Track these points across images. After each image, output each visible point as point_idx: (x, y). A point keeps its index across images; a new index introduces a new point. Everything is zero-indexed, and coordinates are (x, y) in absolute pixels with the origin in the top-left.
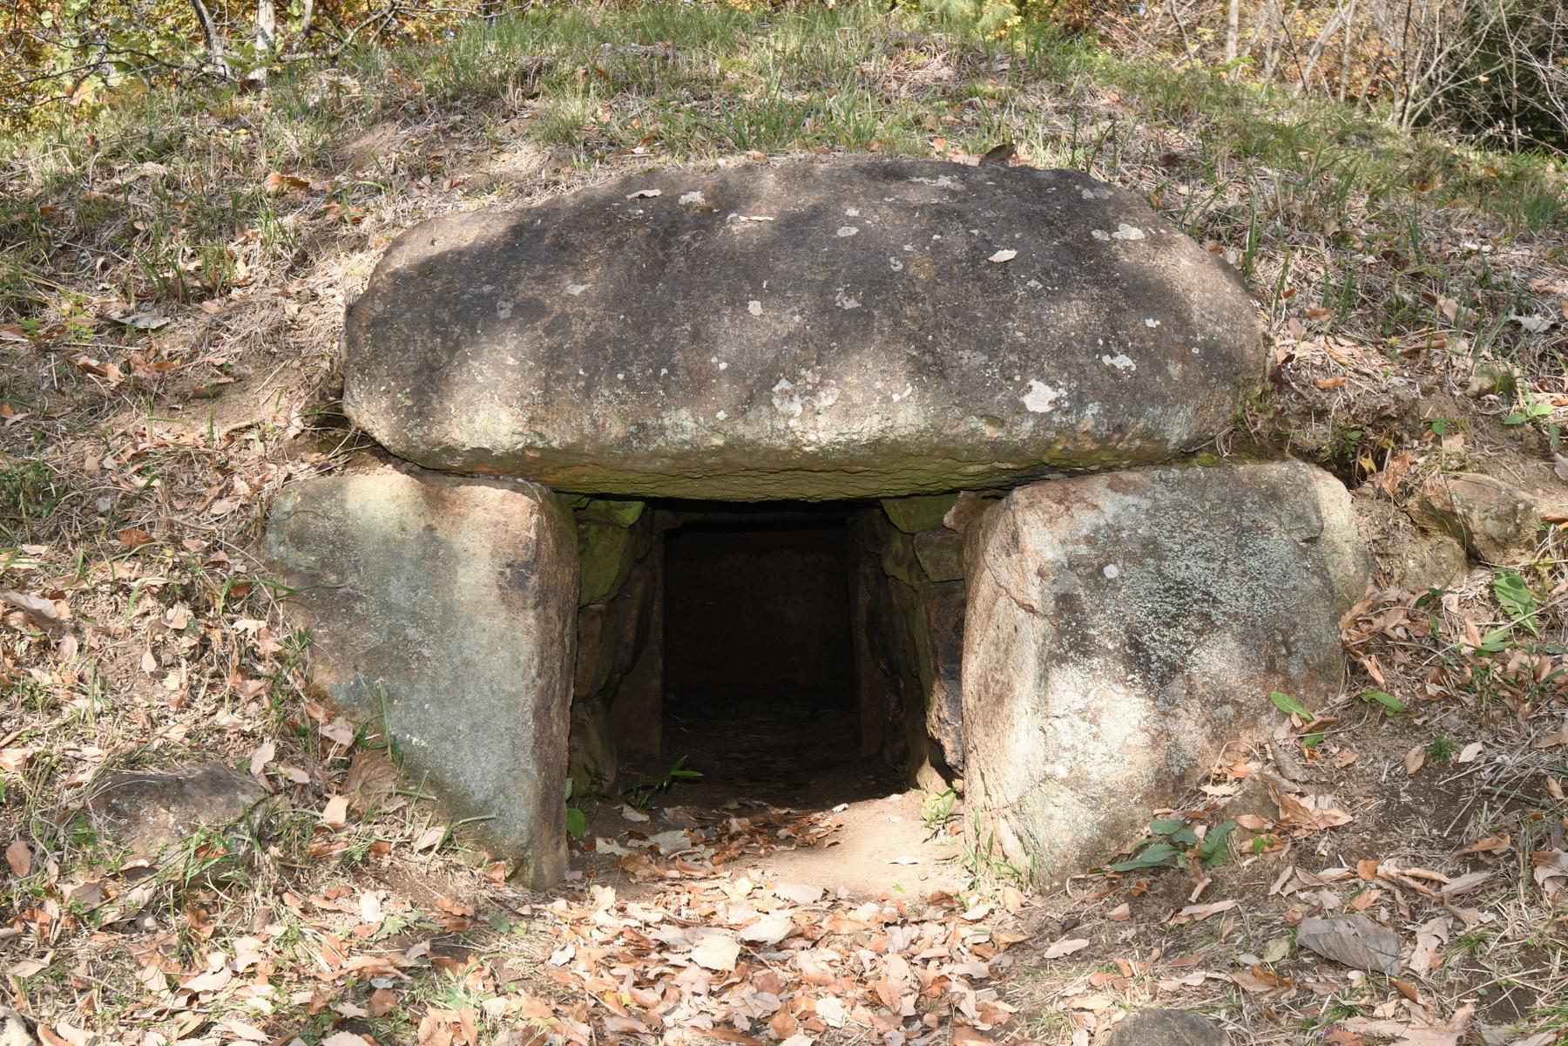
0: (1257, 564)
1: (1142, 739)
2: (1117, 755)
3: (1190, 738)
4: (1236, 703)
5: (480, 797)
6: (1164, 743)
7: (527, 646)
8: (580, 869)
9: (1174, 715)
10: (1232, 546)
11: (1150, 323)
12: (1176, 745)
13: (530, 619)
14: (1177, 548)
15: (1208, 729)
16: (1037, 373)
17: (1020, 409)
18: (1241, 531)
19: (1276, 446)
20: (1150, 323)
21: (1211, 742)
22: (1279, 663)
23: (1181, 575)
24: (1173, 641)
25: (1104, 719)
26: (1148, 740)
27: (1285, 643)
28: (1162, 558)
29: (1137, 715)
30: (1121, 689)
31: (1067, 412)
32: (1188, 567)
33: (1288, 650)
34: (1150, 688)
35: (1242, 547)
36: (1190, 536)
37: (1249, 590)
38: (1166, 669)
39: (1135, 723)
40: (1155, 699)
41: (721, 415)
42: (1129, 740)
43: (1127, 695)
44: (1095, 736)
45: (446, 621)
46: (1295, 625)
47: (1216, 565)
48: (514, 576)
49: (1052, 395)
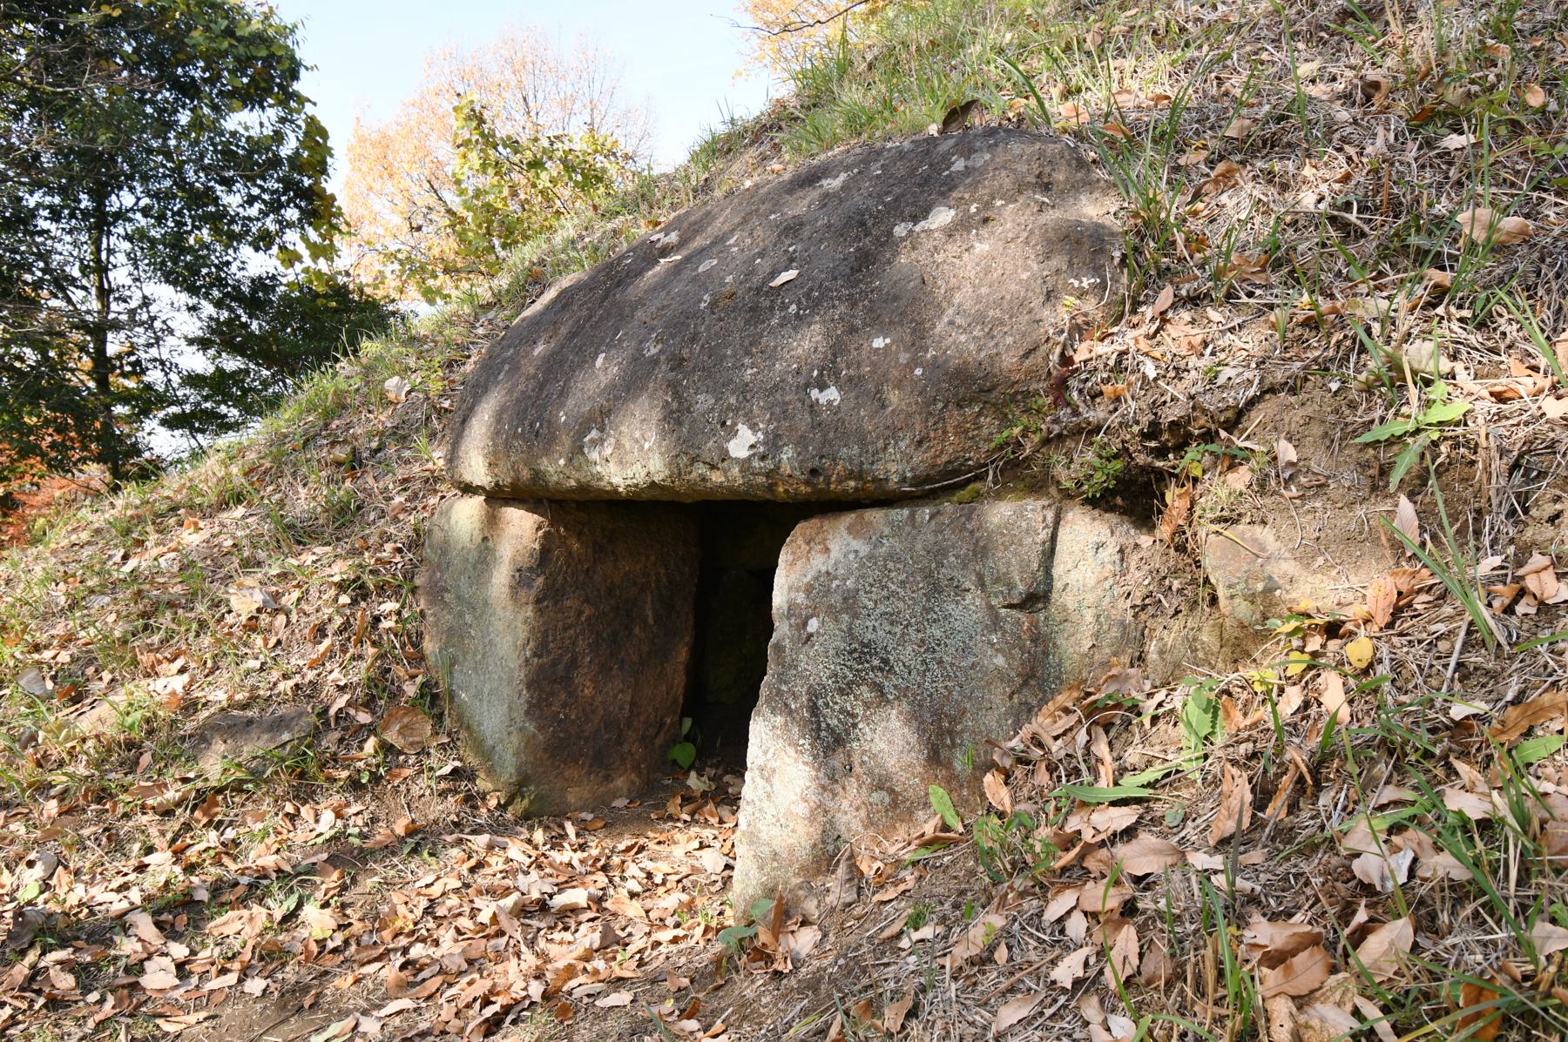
0: (938, 634)
1: (802, 809)
2: (782, 821)
3: (845, 819)
4: (891, 791)
5: (490, 742)
6: (821, 819)
7: (522, 632)
8: (536, 806)
9: (832, 791)
10: (918, 609)
11: (879, 343)
12: (831, 823)
13: (529, 611)
14: (871, 604)
15: (863, 813)
16: (745, 415)
17: (725, 456)
18: (936, 589)
19: (1020, 473)
20: (879, 343)
21: (866, 827)
22: (944, 754)
23: (869, 636)
24: (842, 711)
25: (776, 780)
26: (807, 811)
27: (951, 732)
28: (855, 616)
29: (801, 782)
30: (791, 751)
31: (763, 458)
32: (874, 629)
33: (953, 741)
34: (815, 757)
35: (927, 610)
36: (885, 593)
37: (924, 662)
38: (831, 740)
39: (798, 791)
40: (818, 770)
41: (562, 462)
42: (792, 807)
43: (796, 760)
44: (769, 796)
45: (478, 608)
46: (964, 712)
47: (898, 630)
48: (521, 578)
49: (753, 440)
